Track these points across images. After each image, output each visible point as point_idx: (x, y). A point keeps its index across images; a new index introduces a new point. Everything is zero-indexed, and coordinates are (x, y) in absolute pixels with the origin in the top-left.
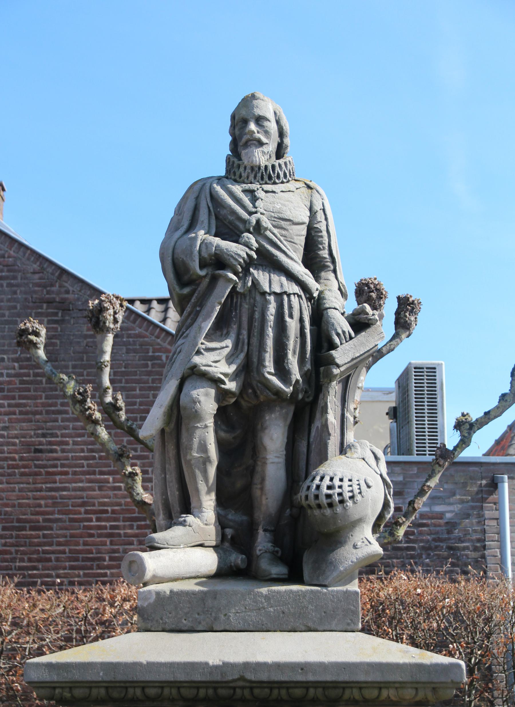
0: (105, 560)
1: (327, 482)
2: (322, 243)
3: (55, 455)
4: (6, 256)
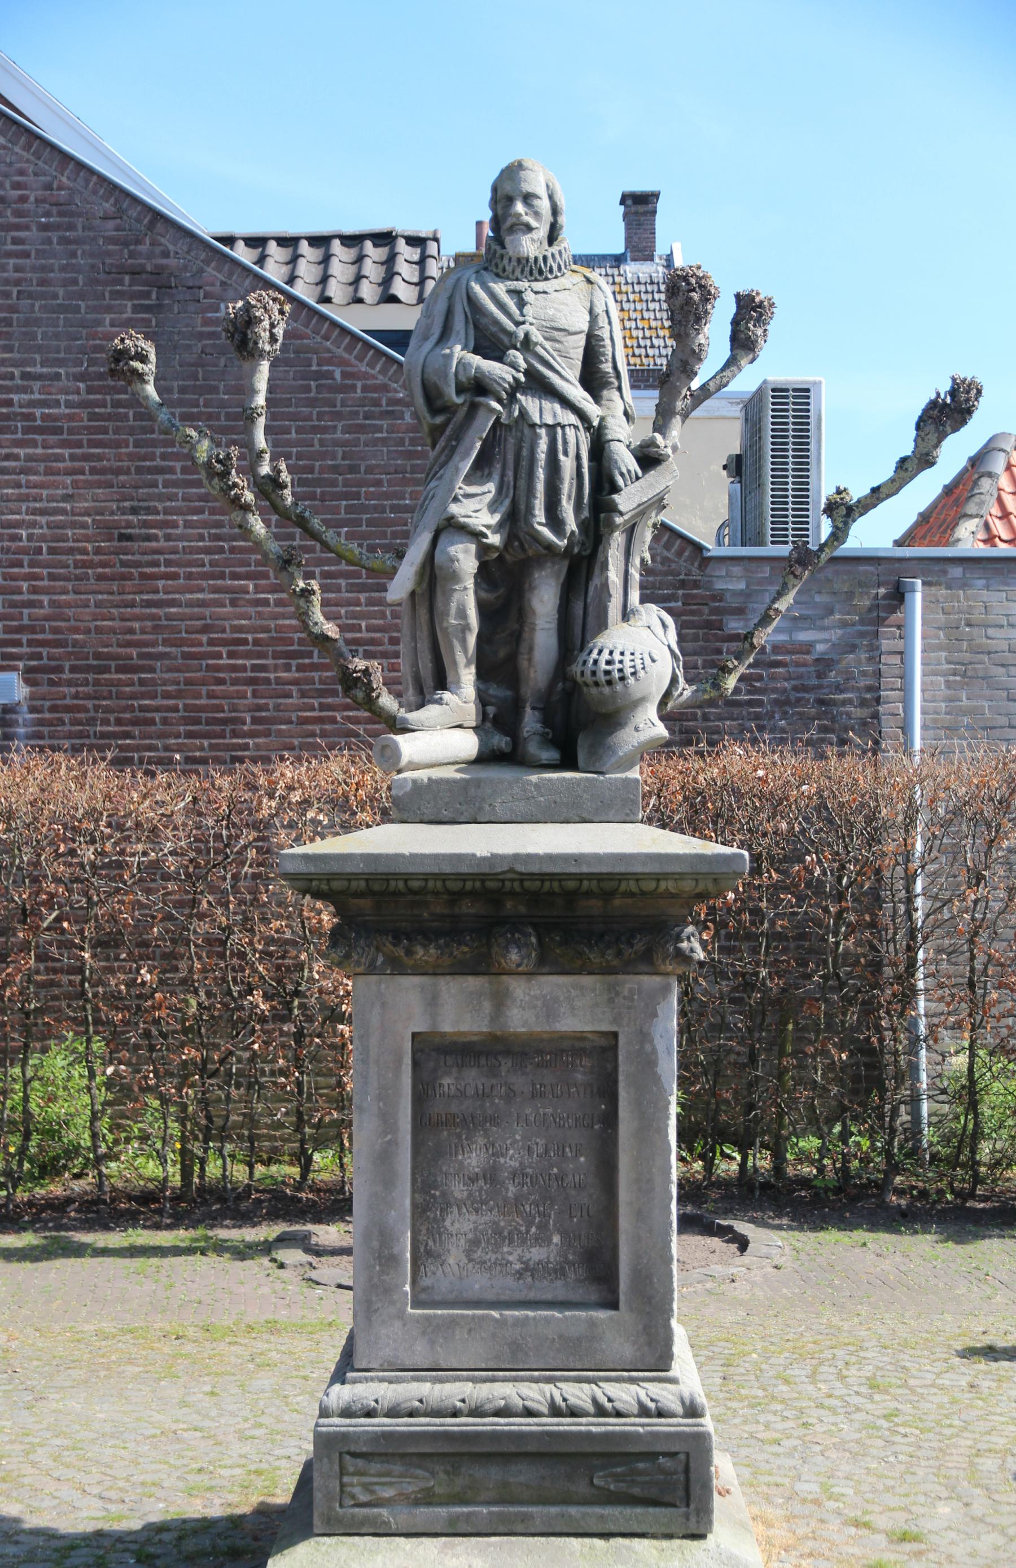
0: (245, 724)
1: (605, 656)
2: (604, 355)
3: (154, 544)
4: (55, 186)
